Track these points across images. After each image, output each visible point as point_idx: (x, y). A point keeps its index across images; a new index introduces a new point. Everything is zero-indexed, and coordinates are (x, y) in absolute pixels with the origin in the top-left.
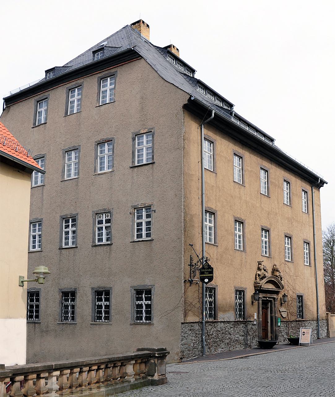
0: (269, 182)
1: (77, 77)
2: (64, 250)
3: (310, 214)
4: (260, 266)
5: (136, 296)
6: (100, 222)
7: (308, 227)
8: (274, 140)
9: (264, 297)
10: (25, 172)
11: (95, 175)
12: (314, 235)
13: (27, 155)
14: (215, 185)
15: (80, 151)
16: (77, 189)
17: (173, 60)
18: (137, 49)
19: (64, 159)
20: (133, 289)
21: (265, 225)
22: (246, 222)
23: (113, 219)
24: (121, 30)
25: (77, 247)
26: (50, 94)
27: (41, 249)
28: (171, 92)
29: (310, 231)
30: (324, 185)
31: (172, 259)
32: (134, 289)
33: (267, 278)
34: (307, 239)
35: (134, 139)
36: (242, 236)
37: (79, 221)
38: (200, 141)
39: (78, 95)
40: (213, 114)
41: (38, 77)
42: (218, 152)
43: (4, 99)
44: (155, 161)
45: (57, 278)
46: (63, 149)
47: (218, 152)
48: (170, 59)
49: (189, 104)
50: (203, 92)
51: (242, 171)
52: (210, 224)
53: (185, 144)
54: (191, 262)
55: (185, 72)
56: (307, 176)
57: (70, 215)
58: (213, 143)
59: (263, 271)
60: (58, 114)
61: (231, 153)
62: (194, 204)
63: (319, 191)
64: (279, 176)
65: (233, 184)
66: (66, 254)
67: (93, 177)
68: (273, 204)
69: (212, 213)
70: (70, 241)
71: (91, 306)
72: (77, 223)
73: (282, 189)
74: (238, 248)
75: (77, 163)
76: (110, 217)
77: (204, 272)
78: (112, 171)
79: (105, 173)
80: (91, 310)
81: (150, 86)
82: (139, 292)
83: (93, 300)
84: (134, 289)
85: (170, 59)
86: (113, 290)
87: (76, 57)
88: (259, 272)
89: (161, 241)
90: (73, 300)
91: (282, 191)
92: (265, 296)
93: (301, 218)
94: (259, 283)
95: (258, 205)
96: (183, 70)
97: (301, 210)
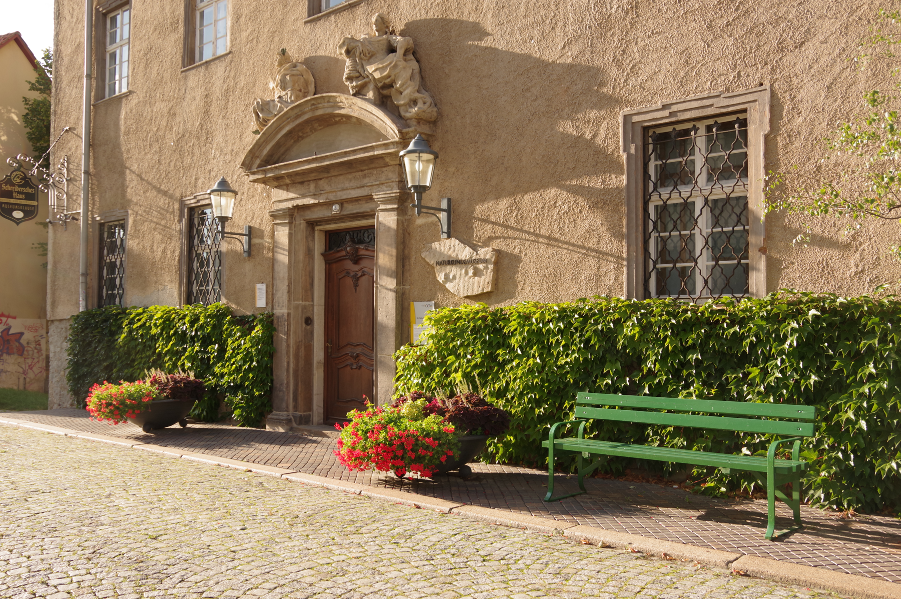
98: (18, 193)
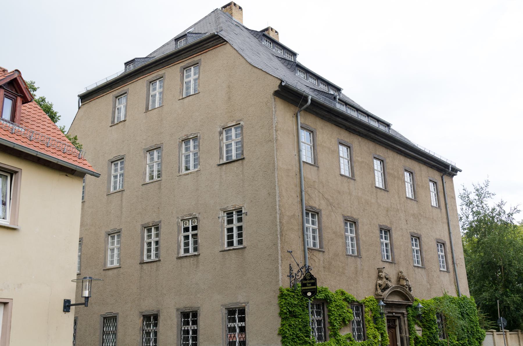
0: (386, 173)
1: (158, 68)
2: (146, 264)
3: (442, 208)
4: (380, 274)
5: (227, 316)
6: (186, 230)
7: (441, 223)
8: (390, 125)
9: (389, 313)
10: (75, 175)
11: (180, 175)
12: (450, 233)
13: (78, 157)
14: (317, 180)
17: (270, 43)
18: (223, 34)
19: (146, 159)
20: (224, 308)
21: (384, 224)
22: (359, 221)
23: (200, 225)
24: (210, 15)
25: (160, 261)
26: (130, 88)
27: (120, 264)
28: (260, 78)
30: (458, 173)
31: (268, 270)
32: (226, 308)
33: (390, 288)
34: (441, 238)
35: (221, 133)
37: (163, 229)
38: (295, 131)
39: (160, 87)
40: (310, 101)
41: (118, 70)
42: (319, 142)
43: (79, 96)
44: (244, 156)
45: (137, 299)
47: (319, 142)
48: (266, 43)
49: (280, 90)
51: (351, 162)
52: (313, 226)
53: (278, 135)
54: (290, 272)
55: (285, 56)
57: (152, 223)
58: (312, 132)
59: (385, 280)
60: (138, 110)
61: (334, 141)
62: (292, 203)
63: (452, 181)
64: (398, 166)
65: (340, 178)
66: (148, 269)
67: (178, 178)
68: (392, 199)
69: (315, 213)
70: (153, 253)
71: (176, 331)
72: (160, 232)
73: (403, 181)
74: (351, 253)
75: (159, 163)
76: (197, 223)
78: (198, 171)
79: (191, 173)
80: (175, 336)
81: (236, 73)
82: (231, 312)
83: (178, 324)
84: (226, 308)
86: (201, 310)
87: (160, 47)
88: (380, 282)
89: (254, 248)
90: (156, 325)
92: (390, 311)
93: (431, 214)
94: (381, 296)
95: (373, 201)
96: (282, 54)
97: (430, 204)
98: (309, 283)
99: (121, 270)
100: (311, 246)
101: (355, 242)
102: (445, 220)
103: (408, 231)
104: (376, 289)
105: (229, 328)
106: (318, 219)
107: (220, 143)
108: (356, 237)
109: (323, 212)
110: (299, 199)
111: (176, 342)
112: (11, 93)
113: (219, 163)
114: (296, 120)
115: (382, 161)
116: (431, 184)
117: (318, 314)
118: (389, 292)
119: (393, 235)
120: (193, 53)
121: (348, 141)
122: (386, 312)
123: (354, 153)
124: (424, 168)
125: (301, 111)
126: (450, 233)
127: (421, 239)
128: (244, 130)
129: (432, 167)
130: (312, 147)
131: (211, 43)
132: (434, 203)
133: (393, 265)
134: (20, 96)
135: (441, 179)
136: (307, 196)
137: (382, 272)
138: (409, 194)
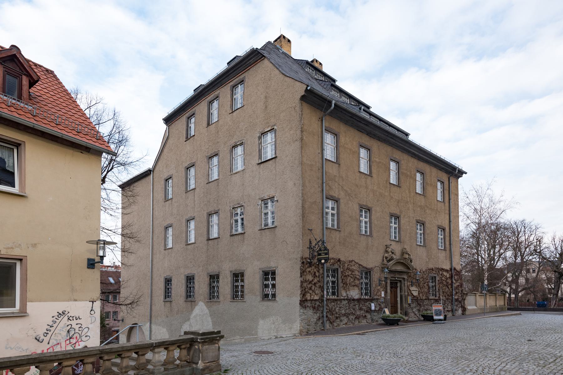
0: (400, 173)
1: (215, 89)
9: (392, 277)
10: (91, 153)
12: (450, 222)
14: (338, 175)
15: (219, 156)
16: (218, 189)
17: (313, 71)
21: (394, 212)
22: (373, 209)
29: (446, 218)
30: (463, 175)
33: (394, 260)
36: (368, 222)
38: (320, 133)
40: (333, 105)
42: (342, 144)
43: (163, 119)
46: (207, 156)
50: (338, 95)
51: (369, 162)
52: (332, 211)
56: (444, 167)
59: (390, 253)
62: (314, 192)
65: (359, 174)
67: (230, 176)
68: (403, 193)
71: (230, 286)
74: (364, 233)
77: (321, 254)
80: (230, 289)
82: (266, 274)
85: (310, 71)
88: (386, 255)
91: (414, 182)
92: (393, 276)
94: (387, 265)
95: (387, 194)
97: (436, 199)
98: (323, 253)
99: (196, 245)
100: (330, 226)
101: (368, 225)
102: (447, 212)
103: (415, 219)
104: (383, 260)
105: (265, 285)
106: (337, 206)
107: (259, 146)
108: (369, 221)
109: (341, 201)
110: (320, 189)
111: (230, 293)
112: (14, 71)
113: (258, 163)
114: (321, 124)
115: (397, 163)
116: (439, 184)
117: (333, 276)
118: (393, 262)
119: (402, 221)
120: (239, 72)
121: (369, 144)
122: (389, 277)
123: (373, 155)
124: (434, 171)
125: (326, 115)
126: (450, 222)
127: (425, 225)
128: (277, 133)
129: (441, 169)
130: (335, 148)
131: (252, 60)
132: (439, 198)
133: (399, 243)
134: (25, 74)
135: (448, 179)
136: (328, 186)
137: (389, 248)
138: (419, 190)
